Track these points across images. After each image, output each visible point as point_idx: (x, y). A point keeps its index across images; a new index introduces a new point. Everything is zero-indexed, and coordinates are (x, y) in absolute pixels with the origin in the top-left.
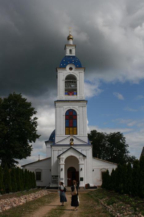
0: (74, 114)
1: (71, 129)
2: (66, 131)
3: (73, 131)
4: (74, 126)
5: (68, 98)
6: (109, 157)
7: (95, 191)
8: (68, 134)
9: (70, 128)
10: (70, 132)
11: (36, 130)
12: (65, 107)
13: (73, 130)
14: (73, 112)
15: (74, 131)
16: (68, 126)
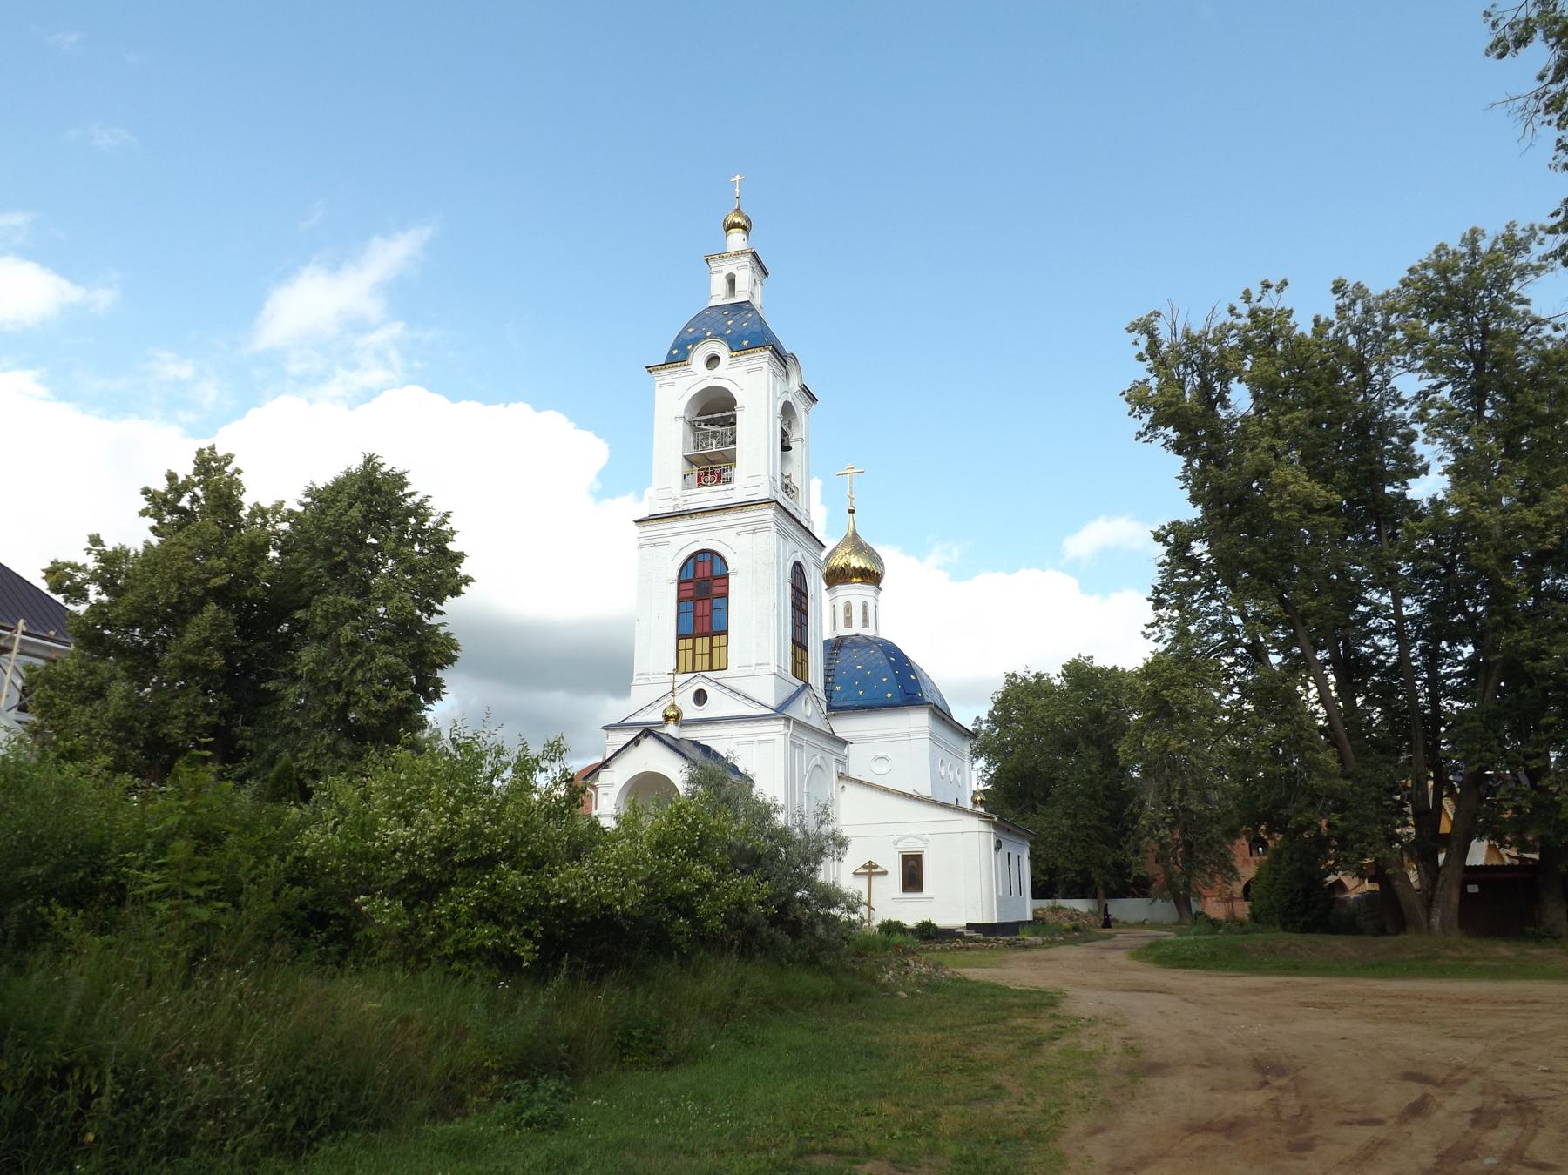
0: (717, 572)
1: (702, 644)
2: (682, 654)
3: (711, 654)
4: (716, 629)
5: (722, 495)
6: (1475, 606)
7: (963, 966)
8: (689, 668)
9: (699, 640)
10: (698, 658)
11: (1447, 477)
12: (678, 542)
13: (711, 647)
14: (712, 561)
15: (715, 651)
16: (690, 631)
